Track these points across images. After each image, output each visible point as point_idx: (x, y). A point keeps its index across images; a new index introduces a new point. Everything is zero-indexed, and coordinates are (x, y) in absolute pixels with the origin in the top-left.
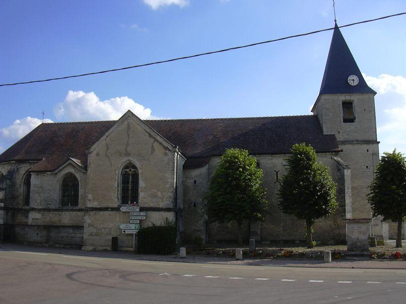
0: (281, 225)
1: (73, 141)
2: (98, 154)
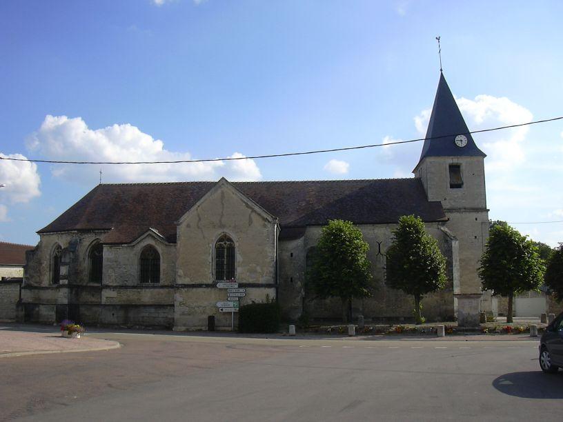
0: (384, 301)
1: (142, 206)
2: (188, 226)
